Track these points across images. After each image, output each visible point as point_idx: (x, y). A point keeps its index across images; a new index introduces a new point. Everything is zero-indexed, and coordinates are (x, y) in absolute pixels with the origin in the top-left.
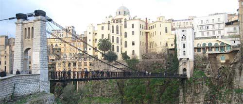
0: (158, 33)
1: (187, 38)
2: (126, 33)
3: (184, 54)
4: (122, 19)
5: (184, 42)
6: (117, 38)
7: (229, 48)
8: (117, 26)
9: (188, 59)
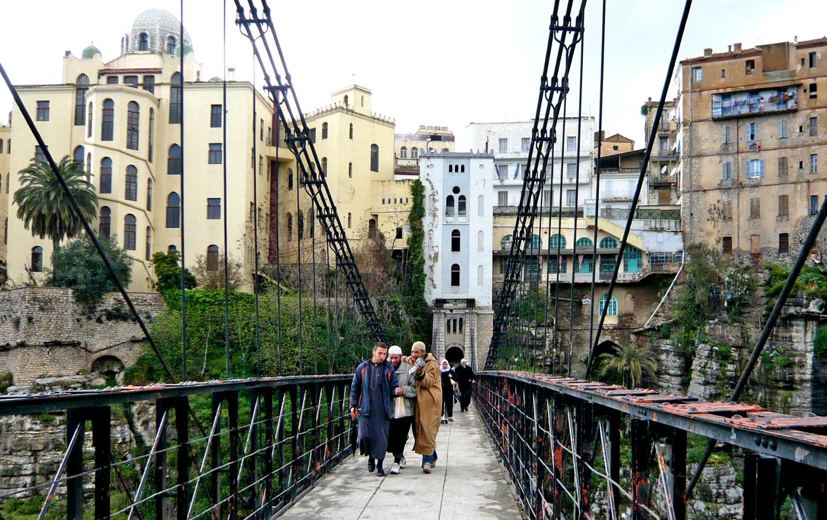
1: (472, 204)
3: (455, 280)
4: (159, 72)
5: (457, 220)
6: (131, 173)
9: (471, 303)
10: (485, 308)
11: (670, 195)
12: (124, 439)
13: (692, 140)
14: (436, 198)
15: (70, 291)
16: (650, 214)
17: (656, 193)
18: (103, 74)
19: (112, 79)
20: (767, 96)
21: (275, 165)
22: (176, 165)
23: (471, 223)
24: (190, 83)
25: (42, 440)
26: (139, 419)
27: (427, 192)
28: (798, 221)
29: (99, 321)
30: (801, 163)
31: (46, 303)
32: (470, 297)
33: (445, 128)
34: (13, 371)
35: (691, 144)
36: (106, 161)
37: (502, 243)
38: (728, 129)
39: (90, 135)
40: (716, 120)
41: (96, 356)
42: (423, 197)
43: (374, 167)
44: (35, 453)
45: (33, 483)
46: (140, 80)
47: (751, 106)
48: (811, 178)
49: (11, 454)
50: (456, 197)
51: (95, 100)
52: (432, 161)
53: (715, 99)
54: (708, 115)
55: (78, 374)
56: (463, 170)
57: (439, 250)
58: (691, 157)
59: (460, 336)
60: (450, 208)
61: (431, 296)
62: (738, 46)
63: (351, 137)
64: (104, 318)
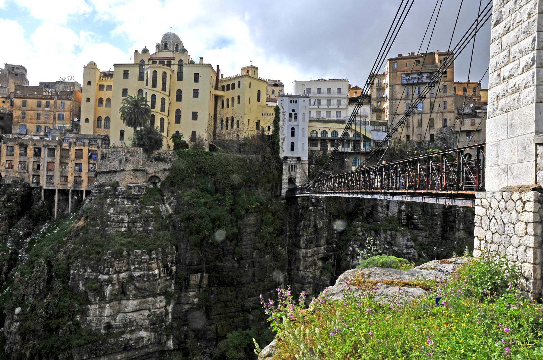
0: (244, 100)
1: (300, 117)
2: (179, 92)
3: (292, 149)
4: (173, 59)
5: (294, 123)
7: (367, 144)
8: (165, 73)
10: (305, 161)
11: (381, 115)
12: (162, 210)
13: (392, 92)
14: (285, 114)
15: (142, 149)
16: (374, 124)
17: (375, 114)
18: (150, 60)
19: (154, 62)
20: (425, 75)
21: (217, 97)
22: (179, 98)
23: (299, 125)
24: (186, 64)
25: (131, 209)
26: (167, 202)
27: (281, 111)
28: (438, 129)
29: (151, 161)
30: (440, 105)
31: (132, 153)
32: (298, 156)
33: (279, 81)
34: (118, 180)
35: (392, 94)
36: (154, 96)
37: (311, 134)
38: (408, 88)
39: (147, 85)
40: (403, 85)
41: (150, 176)
42: (279, 113)
43: (259, 100)
44: (129, 214)
45: (128, 226)
46: (166, 63)
47: (418, 79)
48: (444, 111)
49: (119, 214)
50: (293, 114)
51: (149, 72)
52: (284, 98)
53: (403, 76)
54: (399, 82)
55: (144, 183)
56: (296, 102)
57: (286, 136)
58: (392, 100)
59: (295, 173)
60: (291, 118)
61: (282, 155)
62: (413, 54)
63: (250, 87)
64: (153, 160)
